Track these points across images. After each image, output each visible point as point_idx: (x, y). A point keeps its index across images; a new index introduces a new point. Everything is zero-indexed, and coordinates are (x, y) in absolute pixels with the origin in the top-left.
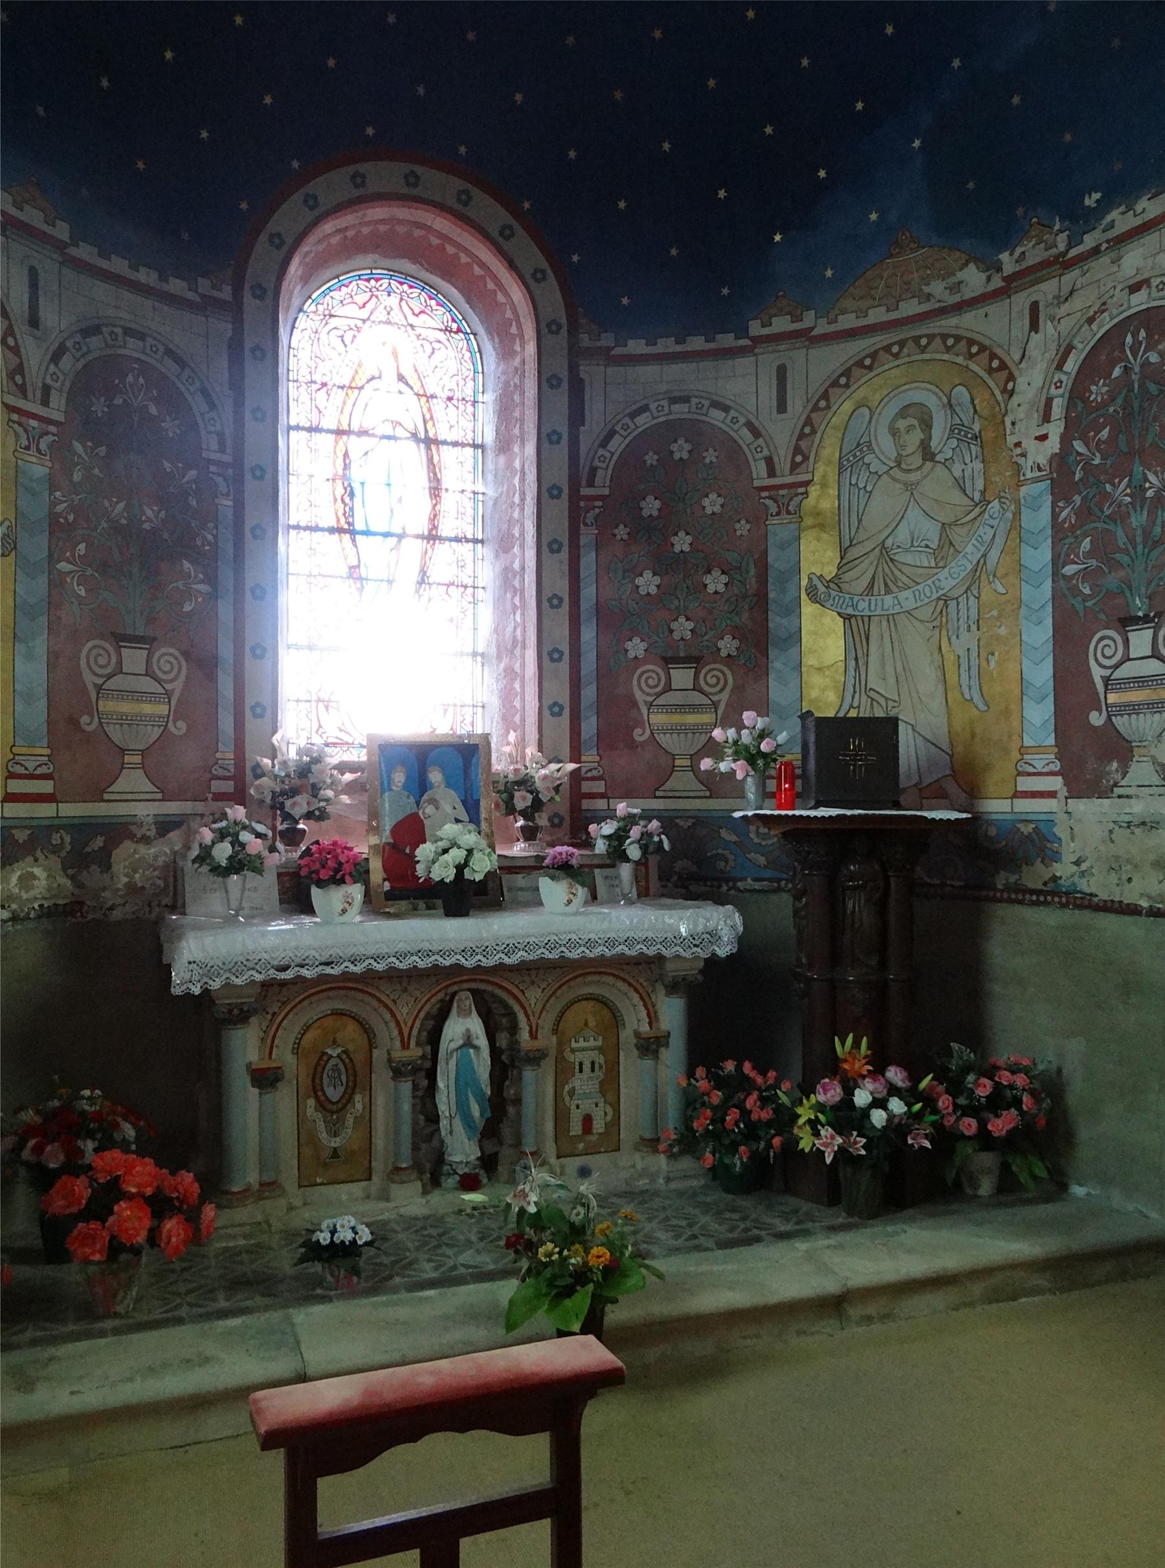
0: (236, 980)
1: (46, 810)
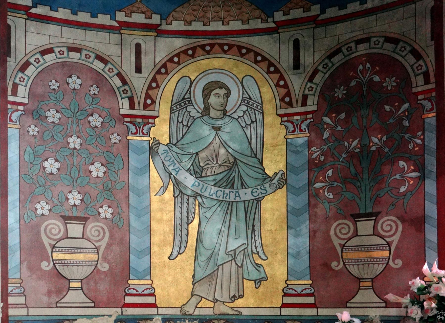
1: (311, 312)
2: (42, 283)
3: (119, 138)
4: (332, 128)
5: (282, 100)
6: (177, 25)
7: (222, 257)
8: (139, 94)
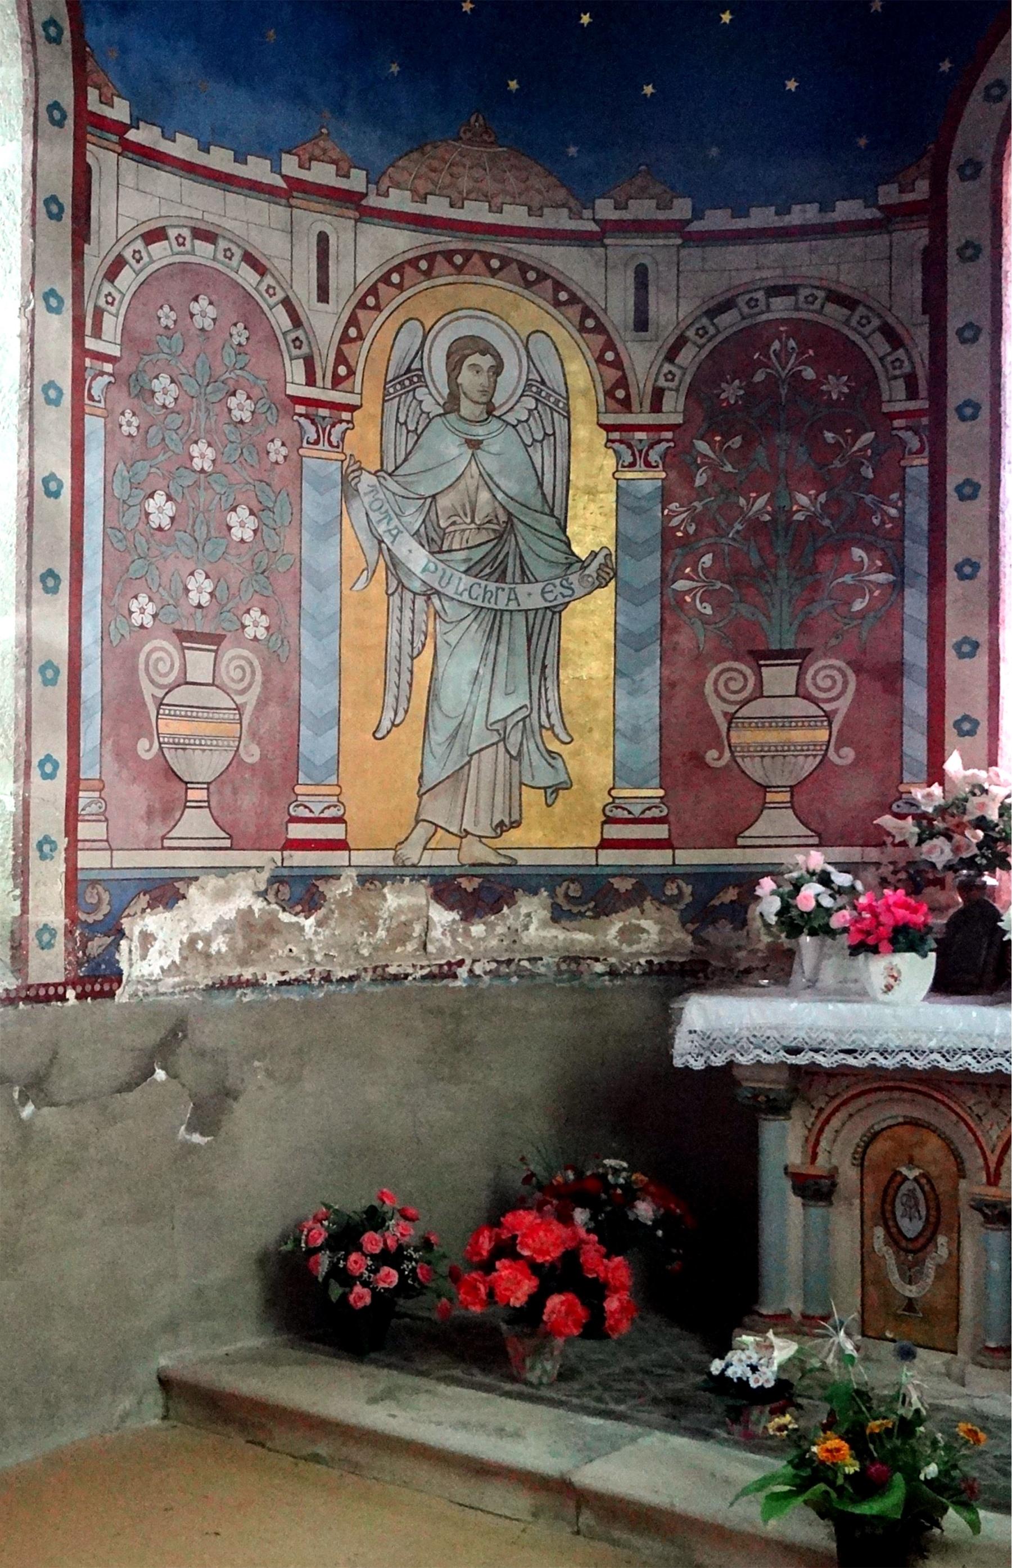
0: (741, 1058)
2: (137, 789)
3: (284, 451)
4: (715, 469)
5: (609, 394)
6: (398, 200)
7: (478, 736)
8: (324, 352)
